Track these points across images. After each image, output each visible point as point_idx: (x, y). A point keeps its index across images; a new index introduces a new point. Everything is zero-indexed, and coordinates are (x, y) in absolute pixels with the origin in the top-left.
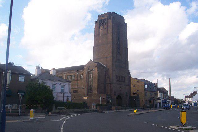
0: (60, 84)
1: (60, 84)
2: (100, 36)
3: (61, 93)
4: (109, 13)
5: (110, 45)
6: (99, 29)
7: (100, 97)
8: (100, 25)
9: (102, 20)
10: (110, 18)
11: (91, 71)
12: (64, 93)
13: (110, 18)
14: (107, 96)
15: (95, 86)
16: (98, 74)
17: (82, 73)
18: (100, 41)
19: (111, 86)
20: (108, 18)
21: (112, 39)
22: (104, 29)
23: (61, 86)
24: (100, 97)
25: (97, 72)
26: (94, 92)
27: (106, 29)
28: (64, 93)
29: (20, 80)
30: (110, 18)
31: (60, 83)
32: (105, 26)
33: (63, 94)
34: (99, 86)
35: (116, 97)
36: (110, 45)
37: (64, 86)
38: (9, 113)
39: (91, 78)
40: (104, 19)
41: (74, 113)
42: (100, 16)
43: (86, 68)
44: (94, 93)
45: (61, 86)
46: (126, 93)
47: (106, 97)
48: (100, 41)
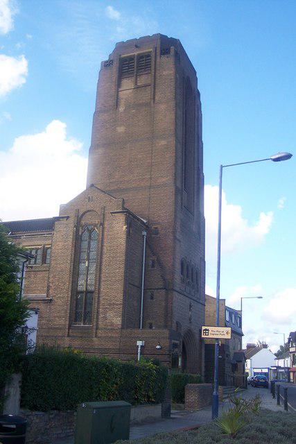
2: (121, 109)
4: (163, 38)
5: (163, 142)
6: (119, 85)
7: (139, 343)
8: (121, 75)
9: (131, 58)
11: (91, 232)
15: (112, 291)
16: (127, 242)
17: (50, 242)
18: (121, 129)
19: (166, 300)
20: (158, 51)
21: (176, 129)
22: (137, 88)
25: (124, 236)
26: (105, 318)
30: (165, 51)
32: (143, 80)
34: (131, 285)
36: (163, 142)
38: (97, 329)
39: (88, 259)
40: (140, 57)
41: (76, 239)
42: (121, 46)
47: (166, 343)
48: (121, 129)
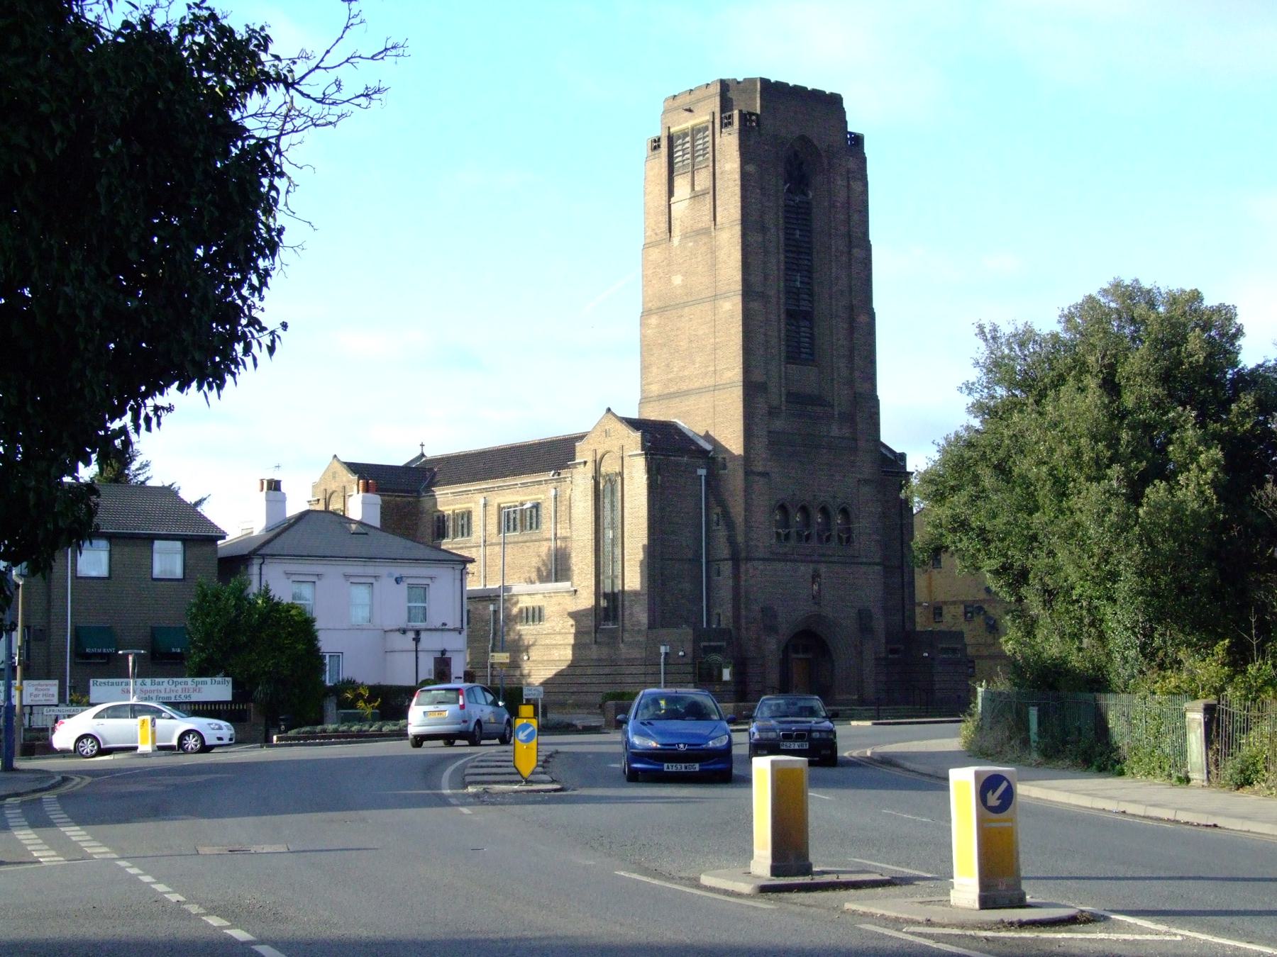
0: (398, 580)
1: (398, 580)
2: (676, 240)
3: (404, 632)
6: (671, 193)
7: (663, 649)
10: (730, 124)
12: (418, 632)
13: (730, 124)
14: (696, 641)
18: (677, 280)
23: (403, 587)
24: (663, 649)
27: (709, 198)
28: (418, 632)
29: (158, 571)
31: (37, 699)
33: (411, 635)
35: (772, 645)
37: (425, 588)
43: (585, 463)
44: (628, 624)
45: (403, 587)
46: (864, 617)
47: (689, 647)
